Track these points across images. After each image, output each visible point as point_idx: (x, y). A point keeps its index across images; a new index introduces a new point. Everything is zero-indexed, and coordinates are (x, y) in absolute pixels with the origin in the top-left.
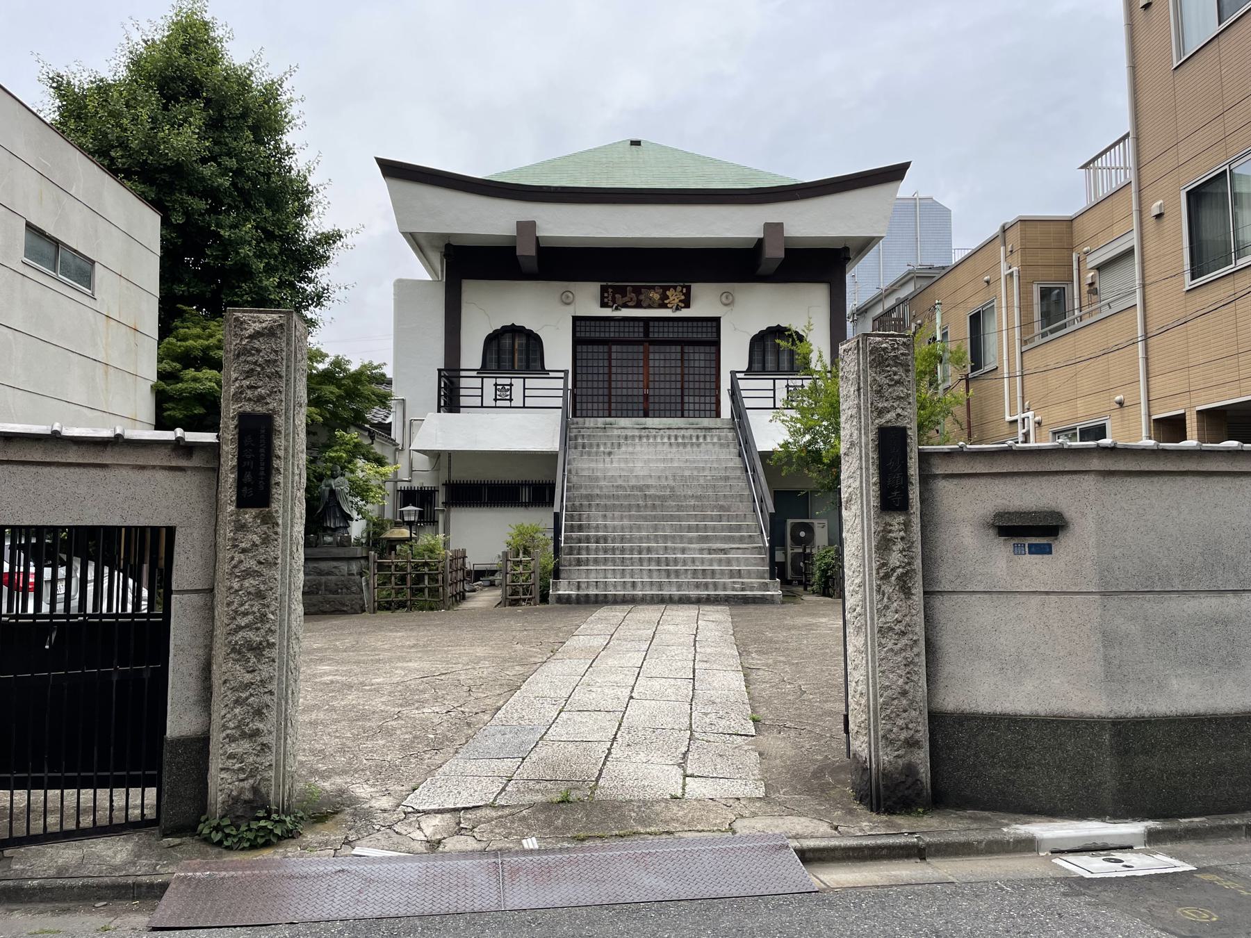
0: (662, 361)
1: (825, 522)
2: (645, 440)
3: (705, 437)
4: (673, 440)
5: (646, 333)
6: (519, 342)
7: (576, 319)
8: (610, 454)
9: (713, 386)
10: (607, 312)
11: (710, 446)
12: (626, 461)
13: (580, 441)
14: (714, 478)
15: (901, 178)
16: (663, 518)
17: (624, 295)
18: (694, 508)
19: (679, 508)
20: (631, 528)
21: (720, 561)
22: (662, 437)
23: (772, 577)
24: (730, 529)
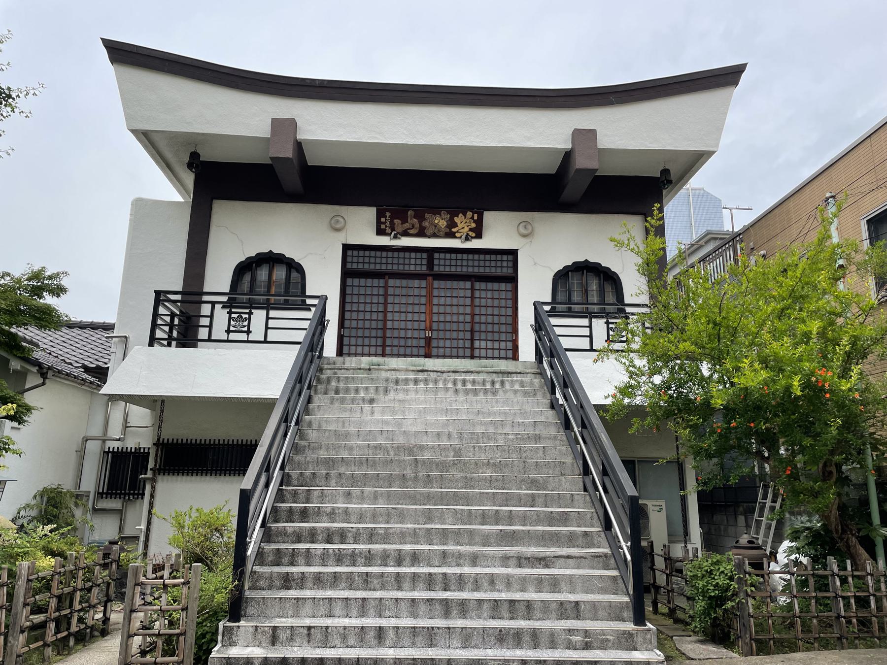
0: (452, 300)
1: (662, 503)
2: (422, 385)
3: (502, 383)
4: (459, 386)
5: (430, 264)
6: (280, 273)
7: (346, 248)
8: (372, 401)
9: (510, 329)
10: (384, 241)
11: (510, 395)
12: (393, 411)
13: (334, 384)
14: (518, 437)
15: (735, 83)
16: (443, 499)
17: (404, 221)
18: (491, 482)
19: (468, 482)
20: (388, 516)
21: (539, 583)
22: (445, 382)
23: (639, 619)
24: (551, 519)
